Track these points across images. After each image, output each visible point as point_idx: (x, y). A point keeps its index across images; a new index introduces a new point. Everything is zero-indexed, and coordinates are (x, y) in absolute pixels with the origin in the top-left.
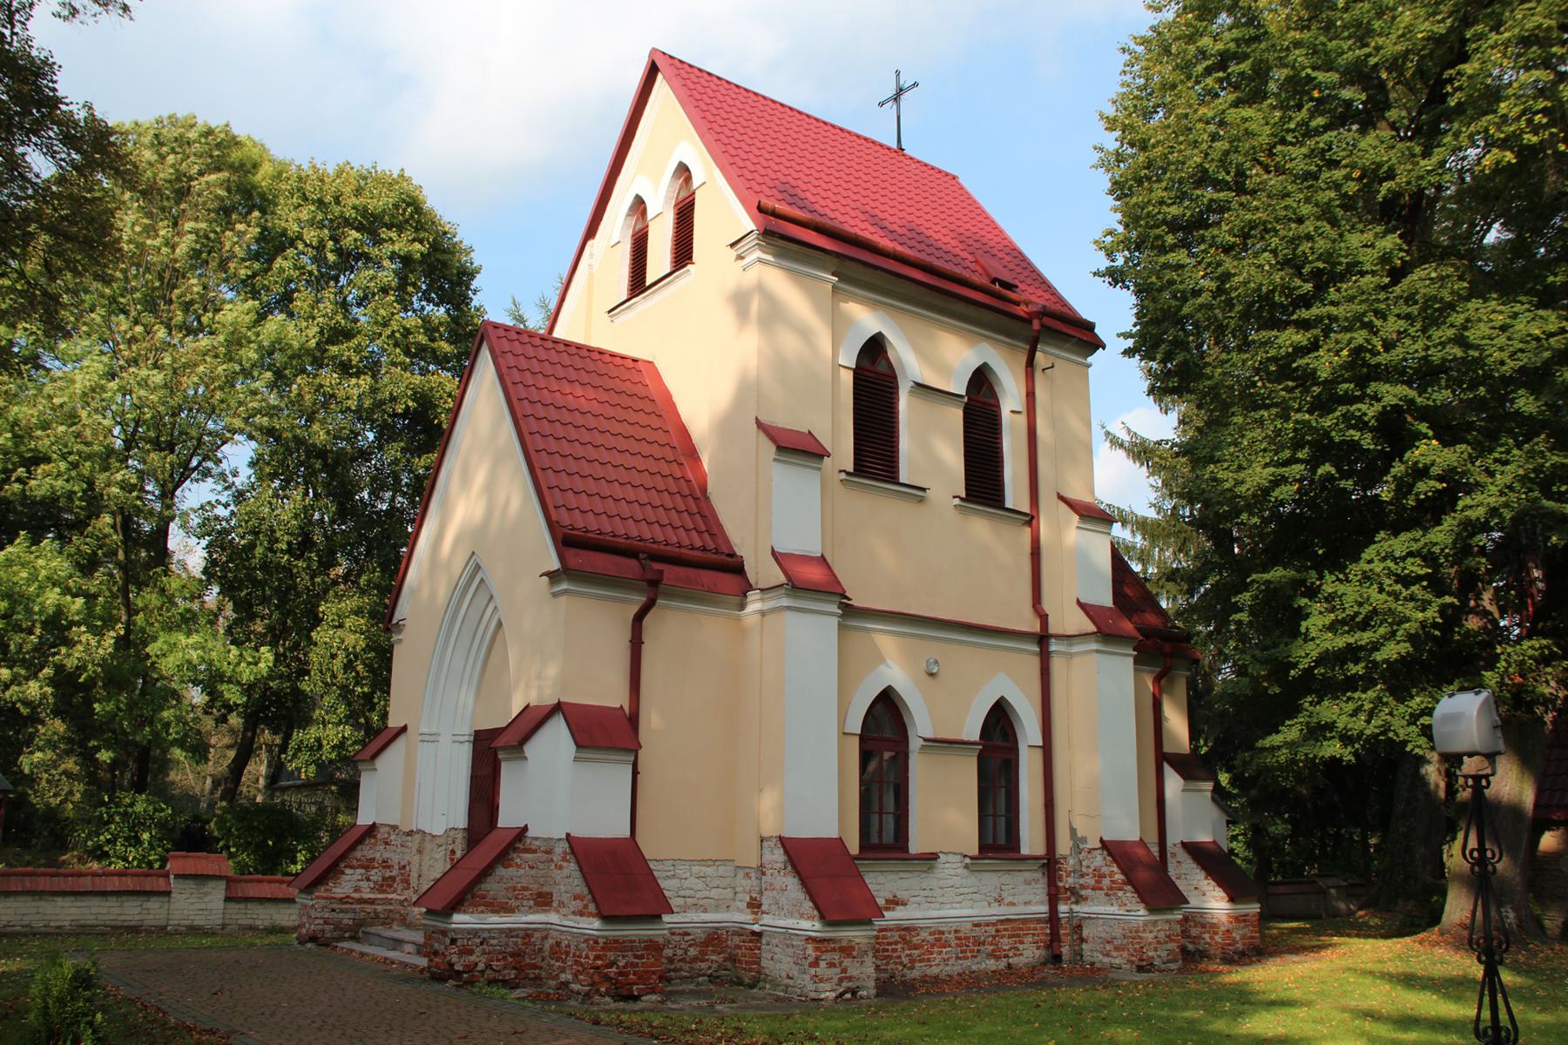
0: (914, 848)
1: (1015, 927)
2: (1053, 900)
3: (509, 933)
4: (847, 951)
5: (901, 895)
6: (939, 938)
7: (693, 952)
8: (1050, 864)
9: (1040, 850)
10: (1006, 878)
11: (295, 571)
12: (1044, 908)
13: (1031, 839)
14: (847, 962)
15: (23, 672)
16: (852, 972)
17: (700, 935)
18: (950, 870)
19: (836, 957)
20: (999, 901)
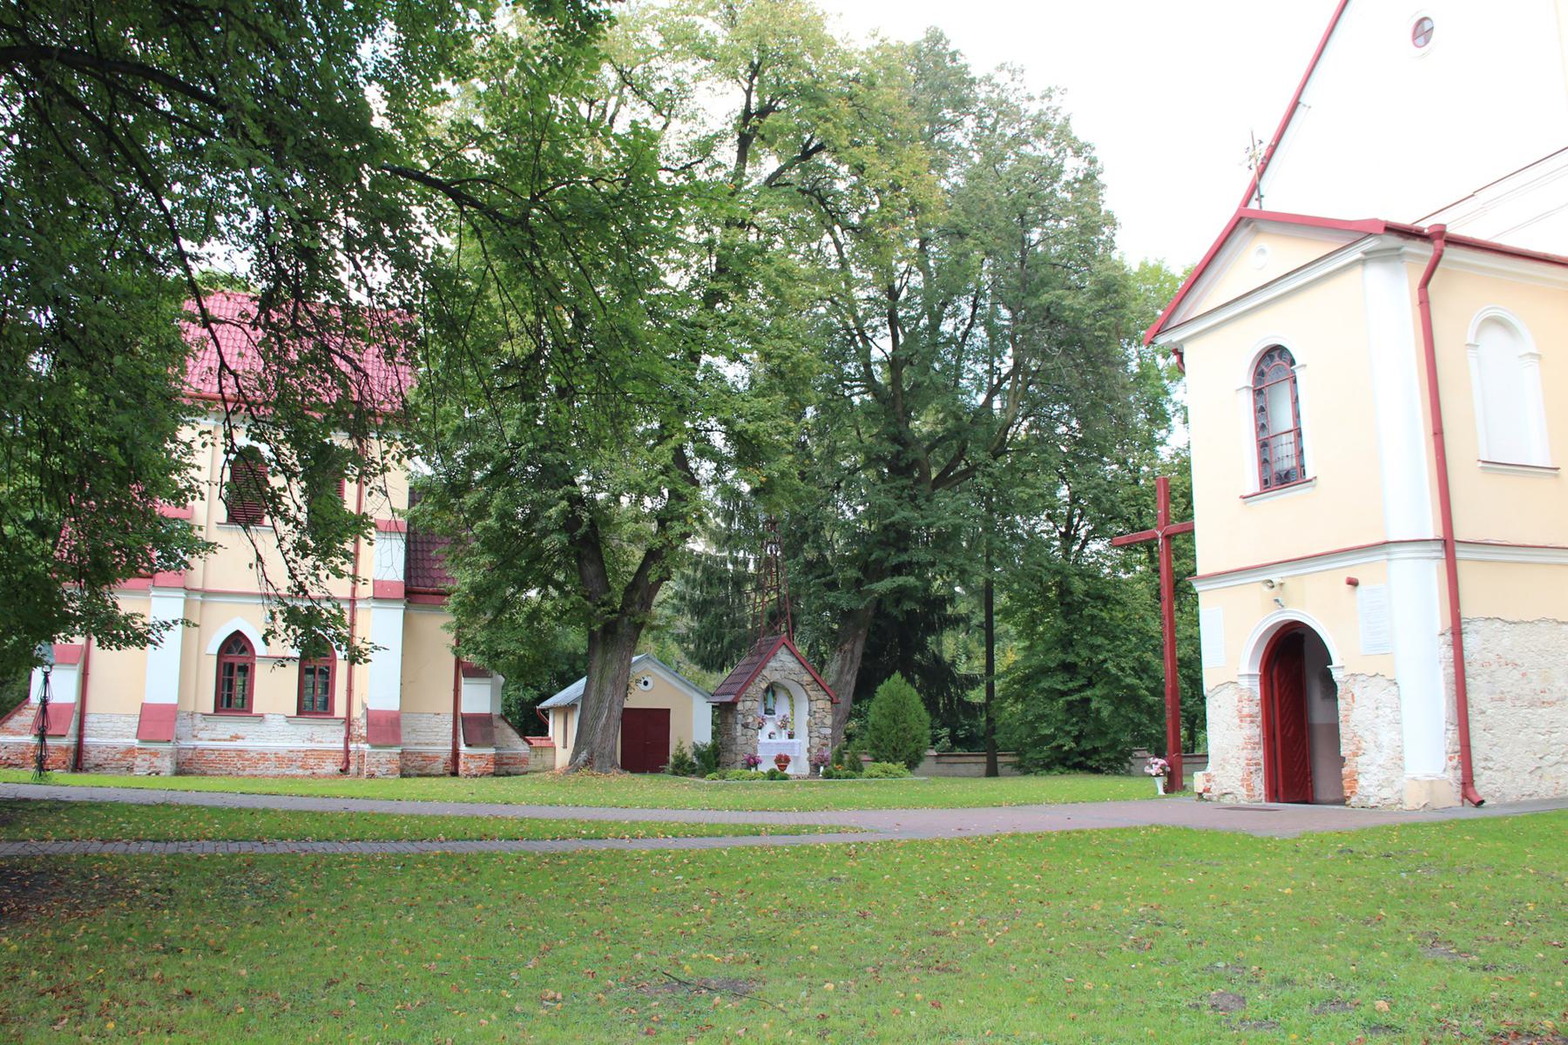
0: (255, 711)
1: (321, 755)
2: (348, 739)
3: (19, 744)
4: (155, 754)
5: (240, 734)
6: (263, 757)
7: (118, 756)
8: (348, 722)
9: (343, 715)
10: (315, 728)
11: (23, 546)
12: (341, 746)
13: (340, 709)
14: (154, 759)
15: (312, 544)
16: (156, 764)
17: (123, 749)
18: (276, 723)
19: (147, 756)
20: (311, 740)
